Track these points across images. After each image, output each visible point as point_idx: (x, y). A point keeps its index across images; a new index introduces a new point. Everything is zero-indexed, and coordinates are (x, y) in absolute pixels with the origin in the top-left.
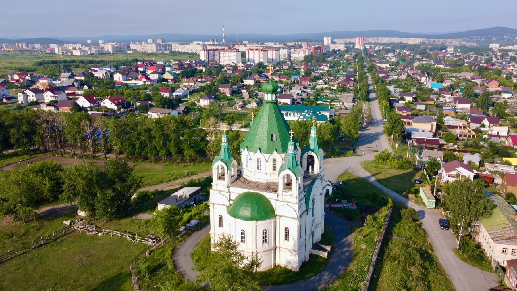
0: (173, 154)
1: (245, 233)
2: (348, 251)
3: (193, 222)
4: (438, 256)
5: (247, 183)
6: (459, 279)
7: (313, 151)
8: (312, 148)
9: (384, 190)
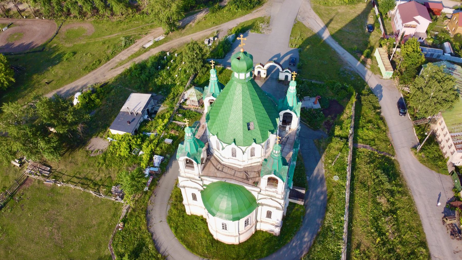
0: (100, 8)
1: (227, 226)
2: (322, 193)
3: (157, 159)
4: (399, 160)
5: (222, 168)
6: (420, 194)
7: (291, 109)
8: (290, 105)
9: (336, 49)
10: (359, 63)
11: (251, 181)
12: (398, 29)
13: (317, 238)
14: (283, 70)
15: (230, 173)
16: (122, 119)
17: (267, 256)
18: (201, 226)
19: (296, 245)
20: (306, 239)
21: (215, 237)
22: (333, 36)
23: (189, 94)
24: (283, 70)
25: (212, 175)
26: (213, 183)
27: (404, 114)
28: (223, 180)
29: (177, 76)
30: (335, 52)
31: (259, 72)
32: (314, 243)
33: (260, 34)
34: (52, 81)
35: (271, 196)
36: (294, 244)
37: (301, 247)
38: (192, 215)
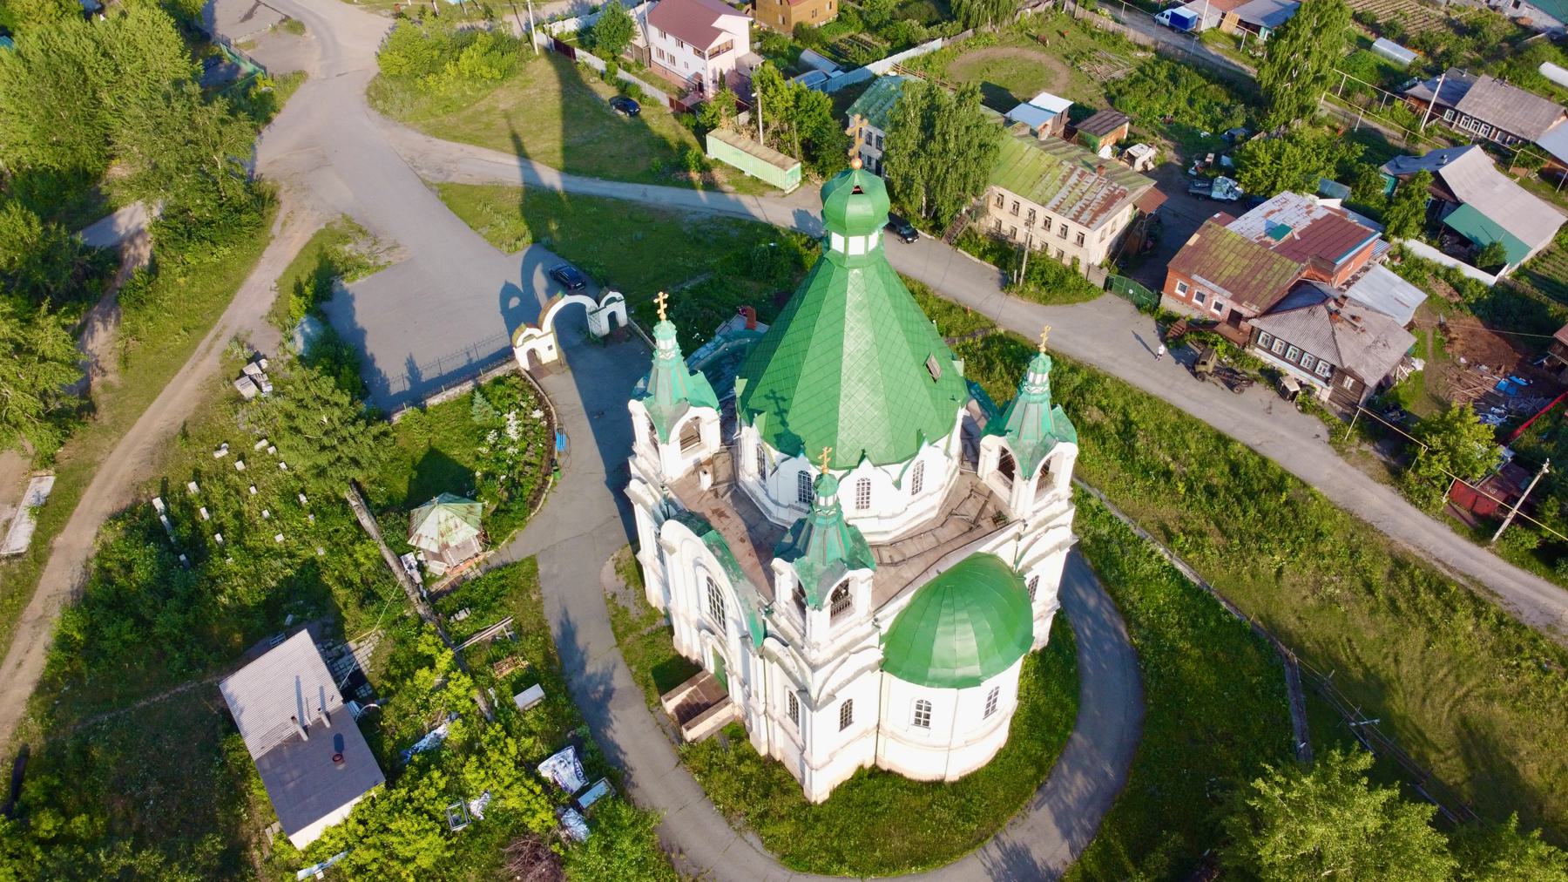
3: (561, 769)
4: (1013, 328)
9: (616, 194)
10: (701, 193)
11: (986, 524)
12: (688, 74)
13: (1104, 580)
14: (598, 303)
15: (926, 547)
16: (295, 773)
17: (1078, 705)
18: (885, 794)
19: (1094, 632)
20: (1092, 602)
21: (953, 775)
22: (567, 171)
23: (435, 535)
24: (598, 303)
25: (897, 588)
26: (904, 614)
27: (914, 234)
28: (933, 575)
29: (280, 538)
30: (621, 203)
31: (532, 354)
32: (1113, 594)
33: (381, 272)
34: (298, 683)
35: (1047, 521)
36: (1088, 632)
37: (1103, 625)
38: (835, 792)
